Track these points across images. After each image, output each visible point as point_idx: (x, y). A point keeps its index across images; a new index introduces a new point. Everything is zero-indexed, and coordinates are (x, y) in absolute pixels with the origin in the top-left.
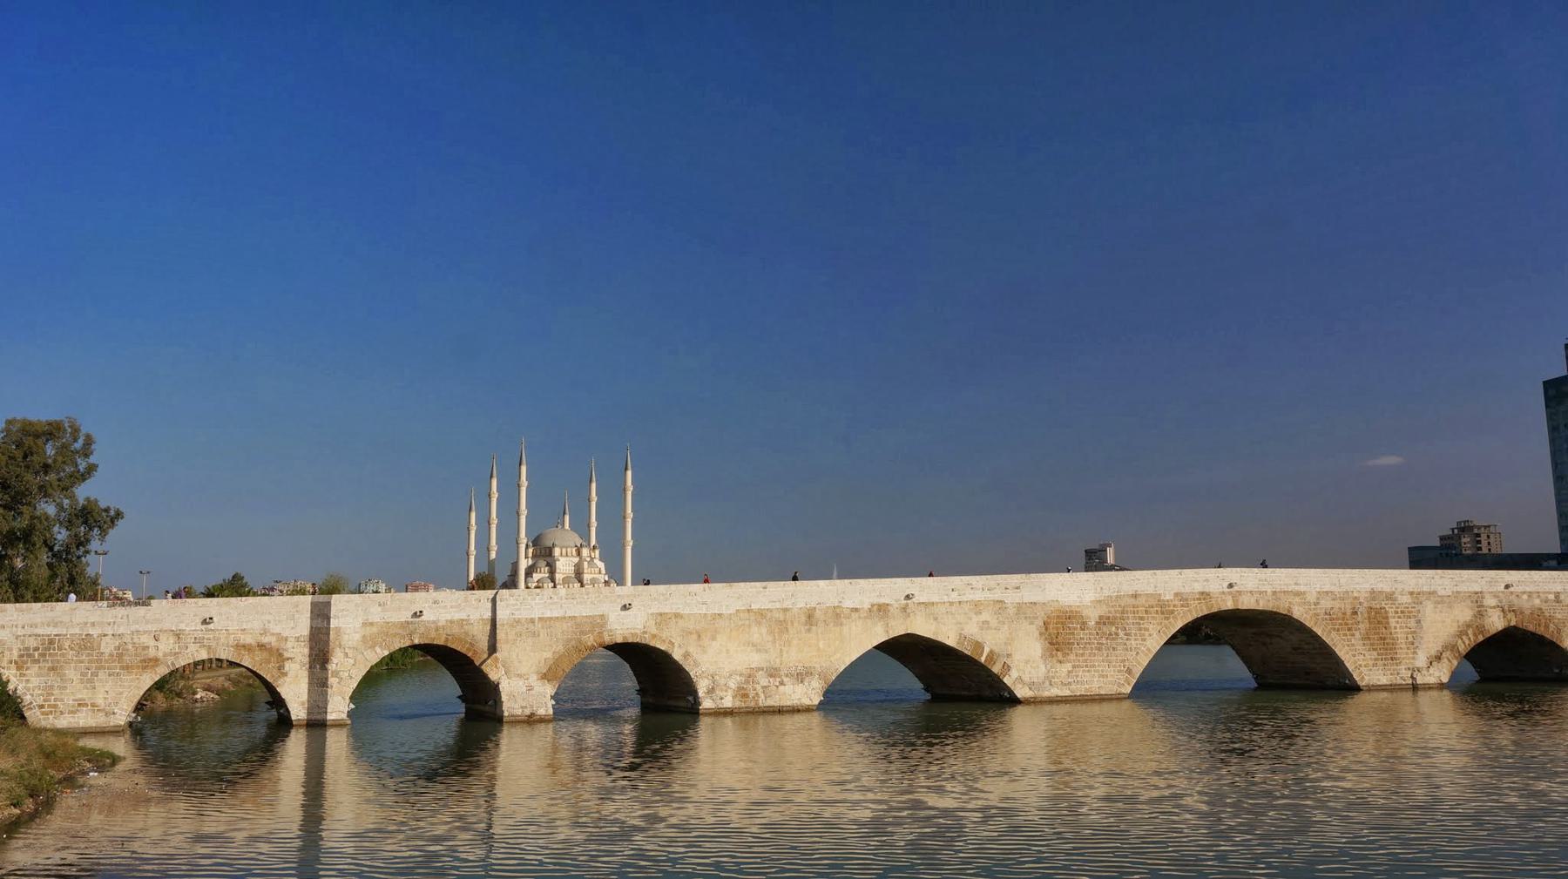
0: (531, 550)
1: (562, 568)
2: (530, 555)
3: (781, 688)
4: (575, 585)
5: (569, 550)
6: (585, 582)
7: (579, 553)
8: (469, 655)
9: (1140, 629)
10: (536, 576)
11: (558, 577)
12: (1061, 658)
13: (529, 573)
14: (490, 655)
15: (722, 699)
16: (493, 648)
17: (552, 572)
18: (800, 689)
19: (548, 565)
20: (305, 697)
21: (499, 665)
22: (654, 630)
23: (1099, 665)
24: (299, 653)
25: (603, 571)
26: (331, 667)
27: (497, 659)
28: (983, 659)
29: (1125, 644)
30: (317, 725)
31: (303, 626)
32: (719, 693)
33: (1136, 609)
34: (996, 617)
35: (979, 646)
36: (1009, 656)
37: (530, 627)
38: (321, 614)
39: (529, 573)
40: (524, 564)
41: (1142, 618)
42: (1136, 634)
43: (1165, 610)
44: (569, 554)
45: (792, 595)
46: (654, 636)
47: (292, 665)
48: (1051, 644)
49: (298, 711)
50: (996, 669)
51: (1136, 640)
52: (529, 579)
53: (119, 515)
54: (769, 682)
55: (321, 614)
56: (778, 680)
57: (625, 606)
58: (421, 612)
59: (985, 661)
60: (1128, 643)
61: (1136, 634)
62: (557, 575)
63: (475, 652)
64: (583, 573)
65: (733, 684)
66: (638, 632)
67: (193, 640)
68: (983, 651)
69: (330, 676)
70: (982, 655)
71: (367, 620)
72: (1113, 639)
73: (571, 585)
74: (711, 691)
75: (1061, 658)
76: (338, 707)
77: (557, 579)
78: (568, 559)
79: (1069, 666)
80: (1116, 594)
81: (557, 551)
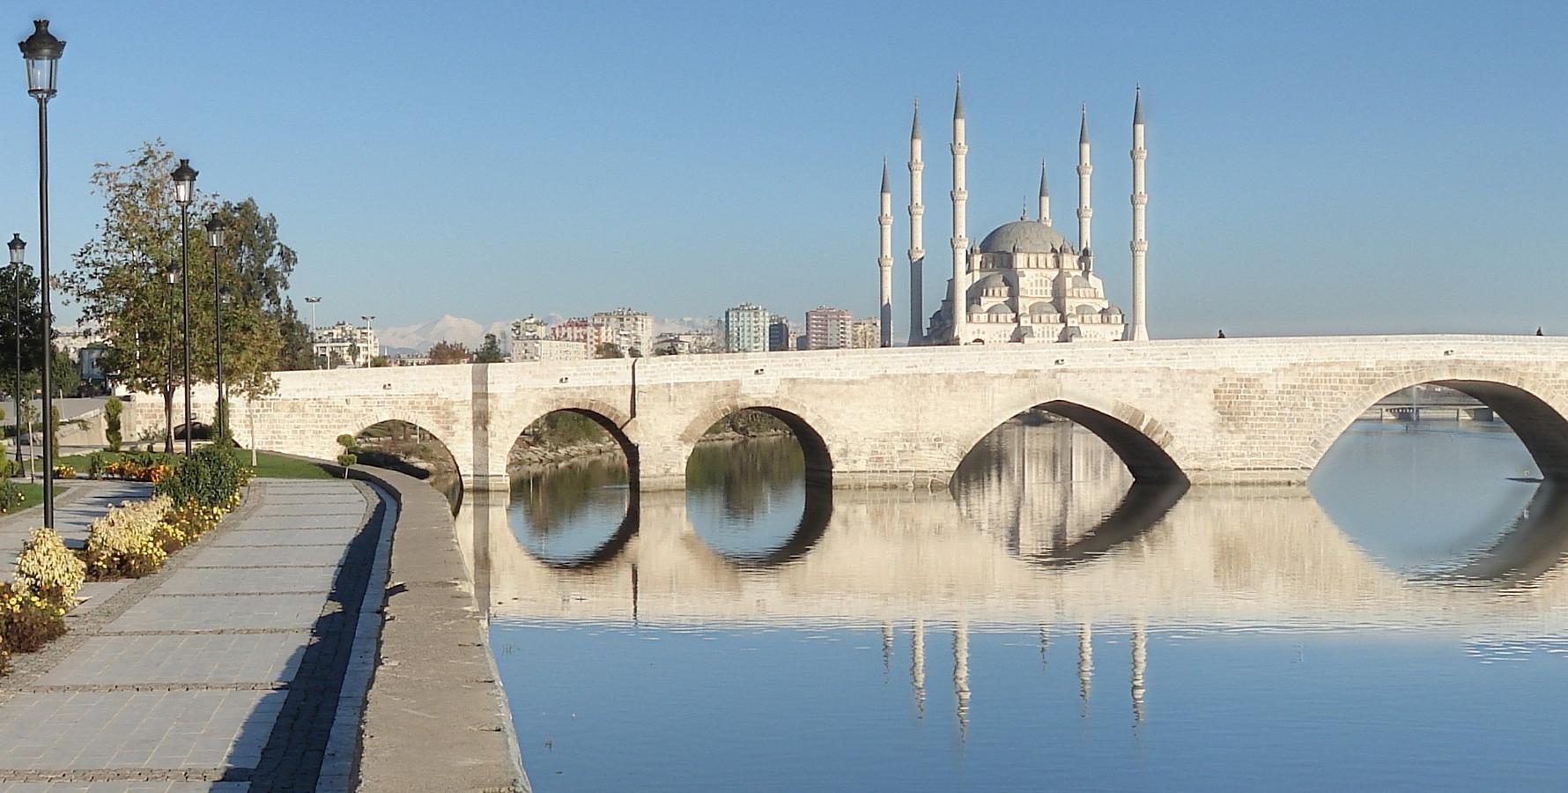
0: (977, 259)
1: (1028, 288)
2: (977, 266)
3: (917, 452)
4: (1052, 316)
5: (1041, 257)
6: (1068, 312)
7: (1058, 265)
8: (612, 419)
9: (1332, 400)
10: (986, 303)
11: (1024, 304)
12: (1233, 429)
13: (974, 297)
14: (632, 418)
15: (855, 462)
16: (633, 414)
17: (1014, 294)
18: (938, 454)
19: (1007, 282)
20: (471, 455)
21: (639, 428)
22: (785, 395)
23: (1279, 437)
24: (466, 415)
25: (1101, 294)
26: (491, 427)
27: (636, 423)
28: (1142, 429)
29: (1312, 415)
30: (482, 491)
31: (467, 391)
32: (851, 456)
33: (1328, 378)
34: (1159, 384)
35: (1139, 415)
36: (1172, 425)
37: (672, 393)
38: (480, 381)
39: (974, 297)
40: (964, 283)
41: (1336, 388)
42: (1326, 405)
43: (1366, 379)
44: (1042, 265)
45: (931, 360)
46: (786, 401)
47: (459, 427)
48: (1222, 413)
49: (468, 482)
50: (1157, 439)
51: (1325, 410)
52: (975, 306)
53: (65, 43)
54: (905, 446)
55: (480, 381)
56: (914, 445)
57: (757, 371)
58: (566, 379)
59: (1144, 430)
60: (1316, 413)
61: (1326, 405)
62: (1020, 299)
63: (617, 417)
64: (1065, 296)
65: (867, 449)
66: (771, 397)
67: (376, 404)
68: (1143, 420)
69: (489, 435)
70: (1141, 424)
71: (520, 386)
72: (1298, 409)
73: (1044, 317)
74: (845, 453)
75: (1233, 429)
76: (498, 466)
77: (1020, 305)
78: (1039, 272)
79: (1243, 437)
80: (1303, 362)
81: (1020, 261)
